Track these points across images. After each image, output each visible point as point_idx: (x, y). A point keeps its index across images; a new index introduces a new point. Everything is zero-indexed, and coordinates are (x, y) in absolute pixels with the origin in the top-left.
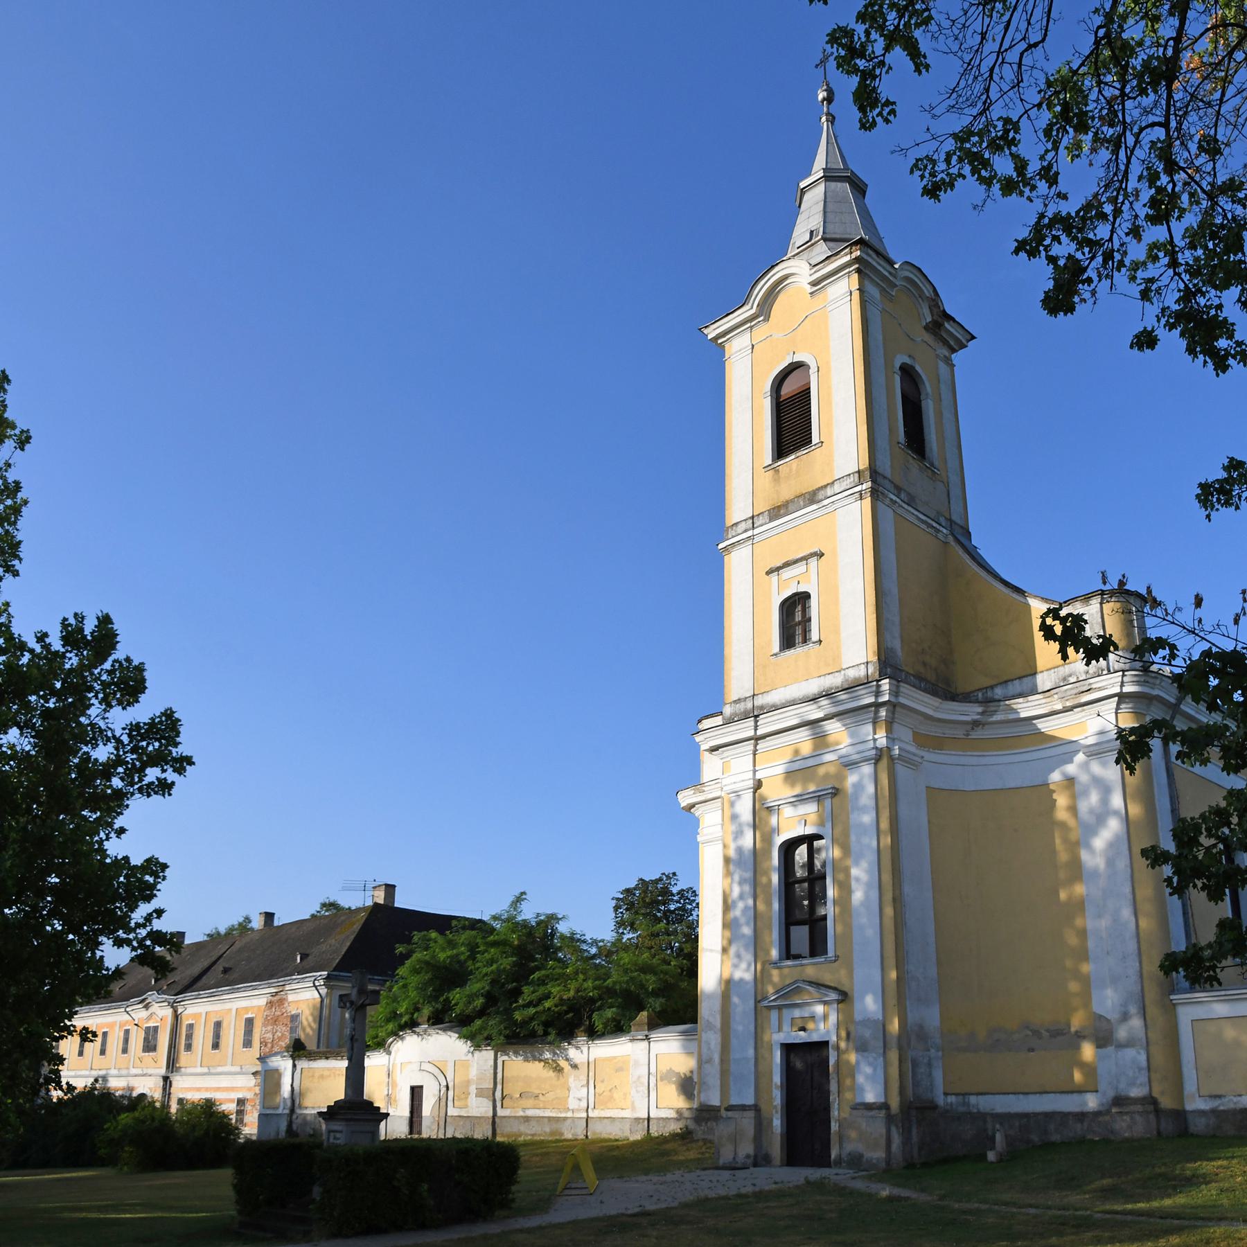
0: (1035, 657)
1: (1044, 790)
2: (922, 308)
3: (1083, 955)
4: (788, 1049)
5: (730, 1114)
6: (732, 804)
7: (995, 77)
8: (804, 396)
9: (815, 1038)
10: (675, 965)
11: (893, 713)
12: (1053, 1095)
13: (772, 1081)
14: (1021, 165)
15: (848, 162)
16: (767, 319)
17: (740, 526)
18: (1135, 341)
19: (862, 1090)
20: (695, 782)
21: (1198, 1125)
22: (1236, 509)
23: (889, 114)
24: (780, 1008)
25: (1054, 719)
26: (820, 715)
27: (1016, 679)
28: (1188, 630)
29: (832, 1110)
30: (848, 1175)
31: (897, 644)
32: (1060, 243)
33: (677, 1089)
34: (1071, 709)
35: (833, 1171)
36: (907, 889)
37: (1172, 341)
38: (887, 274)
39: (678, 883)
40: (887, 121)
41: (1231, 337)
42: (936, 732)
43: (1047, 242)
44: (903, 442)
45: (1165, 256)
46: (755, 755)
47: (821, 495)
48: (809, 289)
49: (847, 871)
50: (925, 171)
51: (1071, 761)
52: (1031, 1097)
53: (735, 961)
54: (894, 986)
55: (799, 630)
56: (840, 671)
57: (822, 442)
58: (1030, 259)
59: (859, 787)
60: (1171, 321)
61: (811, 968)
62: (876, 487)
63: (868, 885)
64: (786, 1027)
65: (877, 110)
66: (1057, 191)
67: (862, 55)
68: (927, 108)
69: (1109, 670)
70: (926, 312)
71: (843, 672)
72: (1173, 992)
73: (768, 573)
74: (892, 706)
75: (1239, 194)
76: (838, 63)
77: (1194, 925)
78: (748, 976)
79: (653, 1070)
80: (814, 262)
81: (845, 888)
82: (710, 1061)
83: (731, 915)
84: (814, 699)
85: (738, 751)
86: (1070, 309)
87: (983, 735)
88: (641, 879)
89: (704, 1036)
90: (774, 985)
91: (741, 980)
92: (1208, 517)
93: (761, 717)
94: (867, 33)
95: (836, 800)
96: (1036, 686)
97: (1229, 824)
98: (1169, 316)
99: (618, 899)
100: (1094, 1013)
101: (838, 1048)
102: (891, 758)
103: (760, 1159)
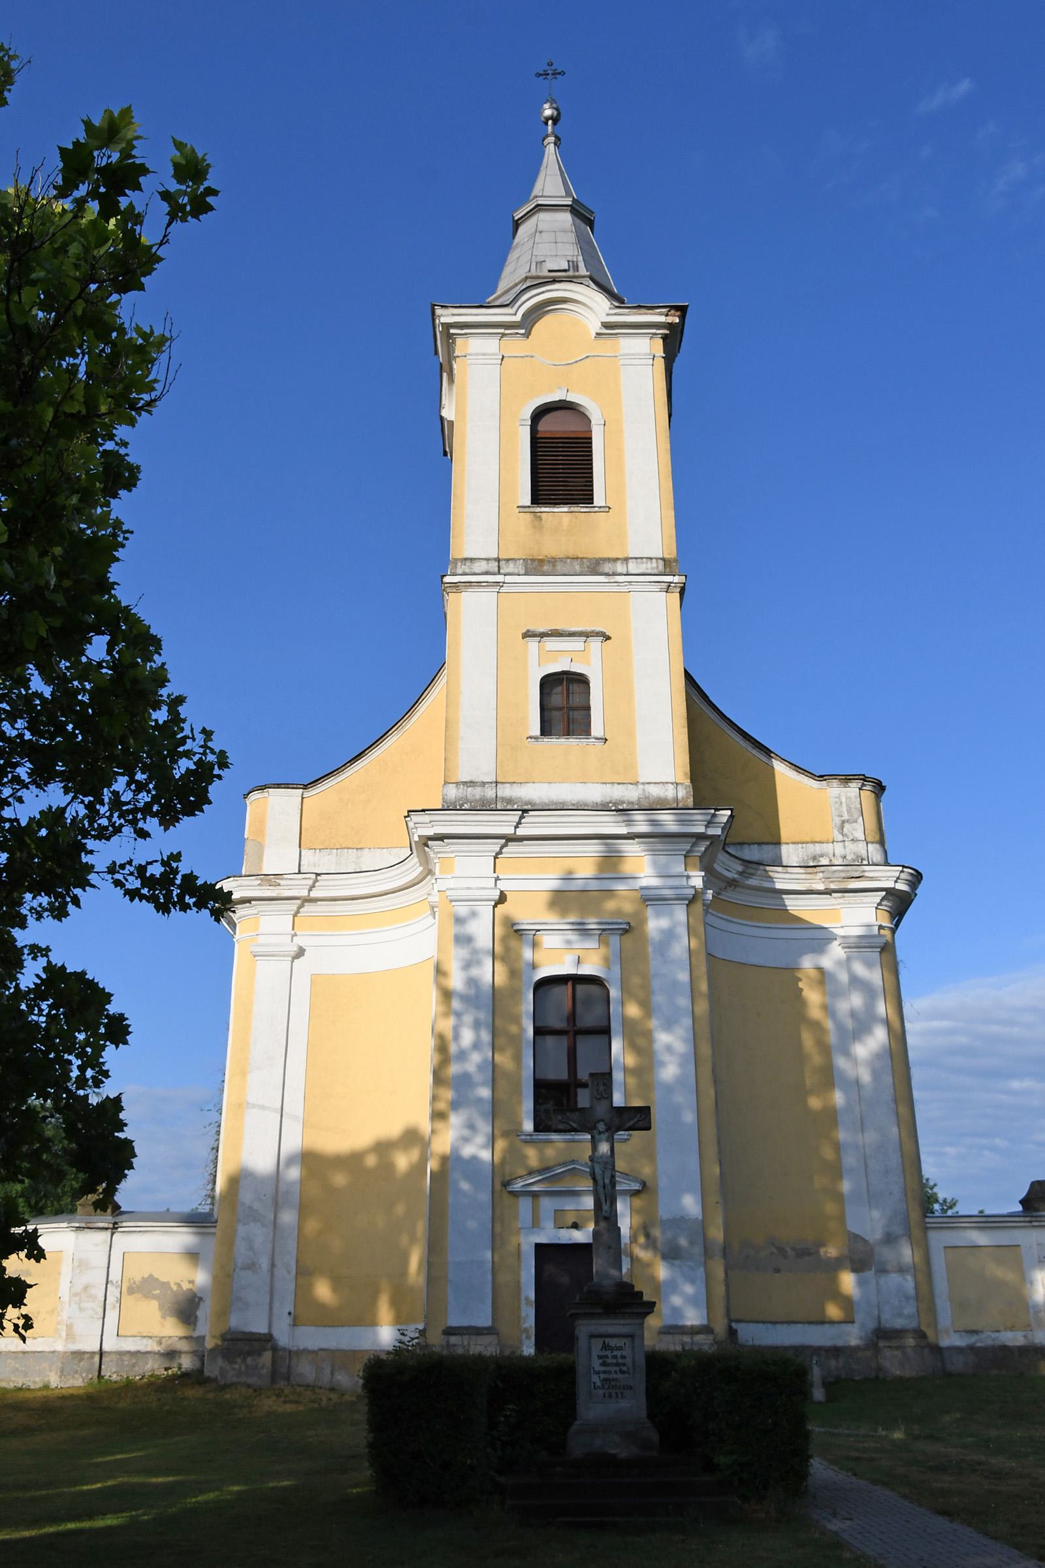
1: (791, 973)
4: (541, 1250)
16: (527, 335)
25: (804, 899)
27: (754, 844)
49: (648, 1035)
52: (778, 1326)
53: (466, 1132)
59: (669, 935)
73: (528, 635)
79: (115, 1275)
91: (474, 1159)
93: (531, 813)
100: (849, 1231)
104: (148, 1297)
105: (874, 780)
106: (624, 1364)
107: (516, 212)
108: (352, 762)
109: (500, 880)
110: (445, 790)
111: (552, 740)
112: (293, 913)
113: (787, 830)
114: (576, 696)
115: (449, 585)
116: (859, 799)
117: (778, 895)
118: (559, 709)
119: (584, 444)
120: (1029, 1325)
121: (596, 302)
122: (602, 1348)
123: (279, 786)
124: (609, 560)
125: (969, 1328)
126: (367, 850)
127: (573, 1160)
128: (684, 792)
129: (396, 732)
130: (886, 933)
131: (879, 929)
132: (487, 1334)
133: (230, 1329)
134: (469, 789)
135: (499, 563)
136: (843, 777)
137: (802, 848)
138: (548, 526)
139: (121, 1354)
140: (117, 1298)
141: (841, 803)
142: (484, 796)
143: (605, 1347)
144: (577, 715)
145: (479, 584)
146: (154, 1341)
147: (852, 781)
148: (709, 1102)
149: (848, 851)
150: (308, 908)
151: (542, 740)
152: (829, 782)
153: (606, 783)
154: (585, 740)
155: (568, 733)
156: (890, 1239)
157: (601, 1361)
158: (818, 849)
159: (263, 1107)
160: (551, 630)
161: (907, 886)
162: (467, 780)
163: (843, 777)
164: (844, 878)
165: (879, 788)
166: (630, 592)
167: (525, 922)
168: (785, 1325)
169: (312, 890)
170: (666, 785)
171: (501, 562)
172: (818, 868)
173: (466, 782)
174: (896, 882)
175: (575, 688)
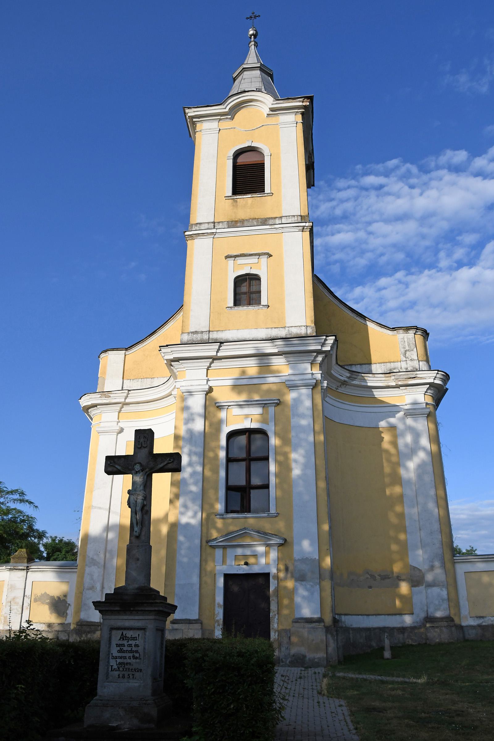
0: (370, 355)
3: (404, 529)
4: (228, 577)
5: (176, 626)
9: (256, 569)
12: (383, 616)
16: (232, 118)
17: (203, 225)
19: (299, 607)
24: (224, 547)
25: (385, 391)
27: (358, 364)
29: (271, 623)
49: (286, 455)
53: (182, 510)
59: (297, 401)
63: (305, 466)
64: (228, 562)
73: (227, 257)
79: (28, 593)
91: (188, 525)
93: (225, 344)
101: (277, 577)
104: (44, 604)
105: (422, 329)
106: (137, 652)
107: (233, 74)
108: (150, 336)
109: (210, 381)
110: (182, 337)
111: (240, 308)
112: (118, 411)
113: (374, 357)
114: (254, 287)
115: (188, 236)
116: (414, 339)
118: (245, 293)
119: (260, 167)
121: (267, 99)
122: (121, 638)
123: (113, 350)
124: (272, 218)
125: (478, 615)
126: (156, 378)
127: (245, 528)
128: (311, 330)
129: (172, 320)
130: (431, 408)
131: (426, 405)
133: (80, 620)
134: (195, 335)
135: (214, 224)
136: (405, 328)
137: (384, 365)
138: (240, 205)
140: (29, 604)
141: (405, 341)
142: (202, 338)
143: (123, 637)
144: (254, 296)
145: (203, 234)
146: (46, 625)
147: (410, 330)
149: (408, 365)
150: (126, 408)
151: (234, 308)
152: (398, 331)
153: (268, 328)
154: (257, 307)
155: (249, 304)
157: (118, 648)
159: (100, 508)
160: (240, 254)
161: (441, 382)
162: (194, 331)
163: (405, 328)
164: (406, 378)
165: (425, 334)
166: (283, 233)
167: (222, 401)
168: (375, 616)
169: (126, 399)
170: (301, 327)
171: (215, 224)
172: (391, 374)
173: (193, 332)
174: (434, 379)
175: (254, 282)
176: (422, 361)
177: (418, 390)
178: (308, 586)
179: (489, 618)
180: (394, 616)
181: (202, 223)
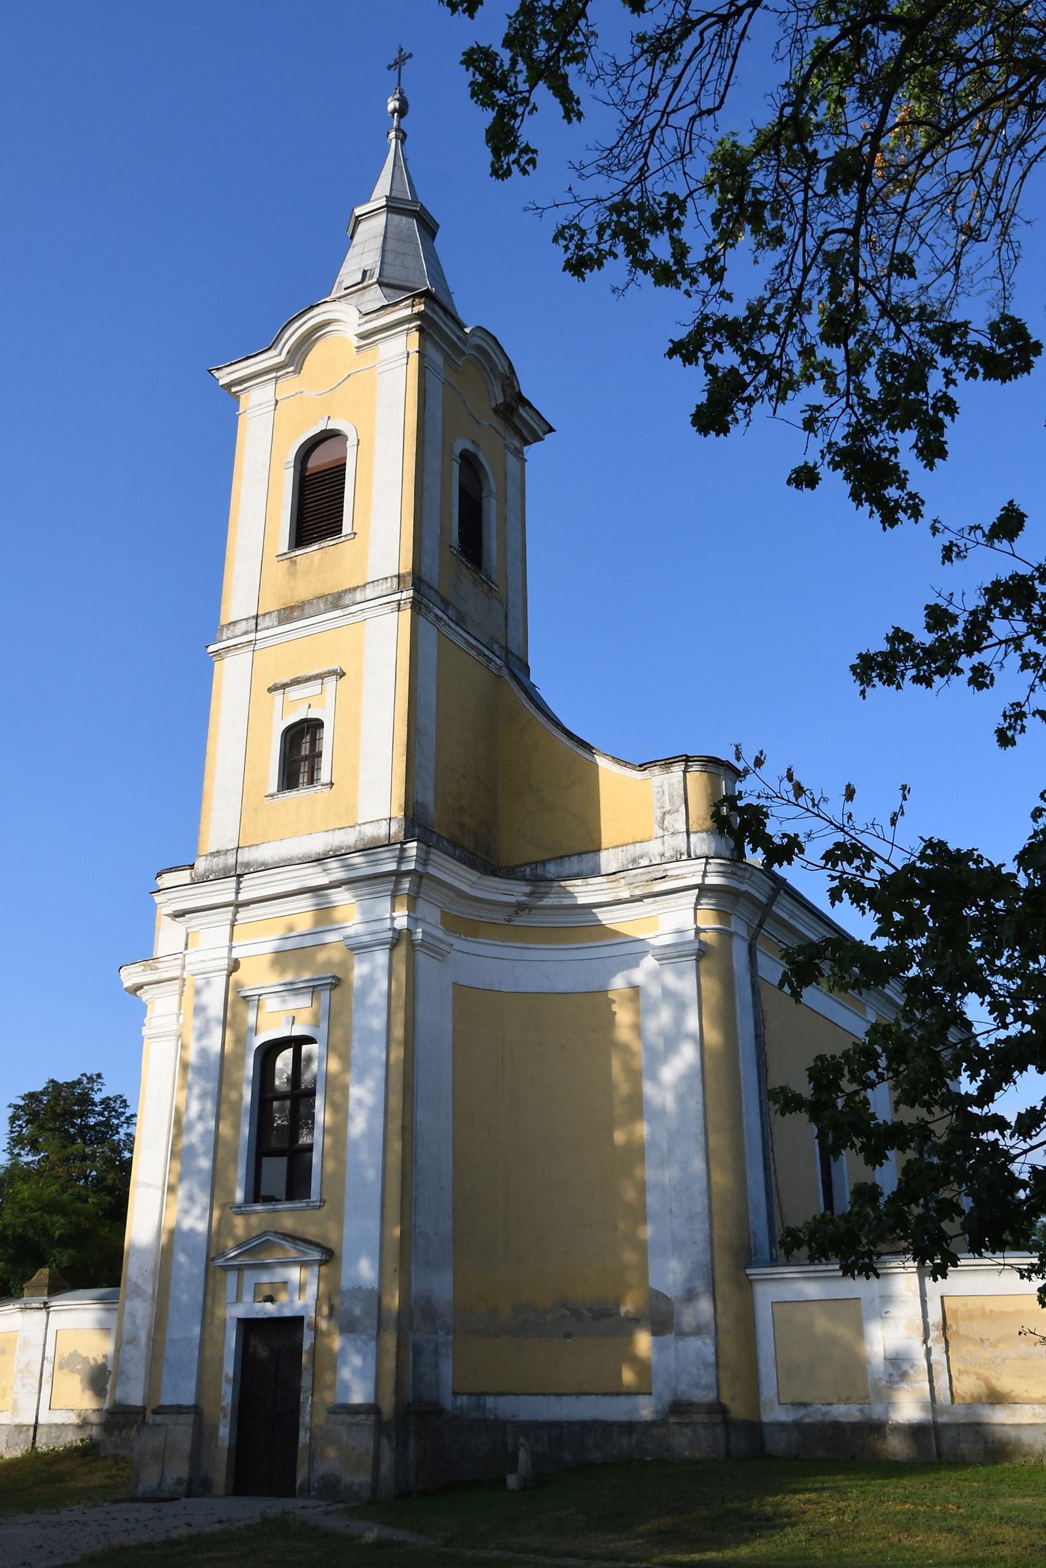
2: (493, 386)
4: (248, 1326)
5: (159, 1419)
6: (198, 992)
7: (656, 141)
8: (337, 473)
9: (287, 1313)
10: (93, 1203)
11: (419, 886)
12: (593, 1397)
13: (222, 1373)
14: (680, 250)
15: (418, 194)
16: (298, 370)
18: (793, 476)
20: (147, 957)
21: (777, 1443)
22: (897, 689)
23: (528, 162)
24: (240, 1269)
25: (618, 910)
26: (324, 881)
27: (574, 855)
28: (836, 826)
29: (301, 1414)
30: (319, 1509)
31: (429, 798)
32: (721, 352)
33: (81, 1382)
34: (641, 899)
35: (299, 1502)
36: (421, 1115)
37: (834, 483)
38: (455, 338)
39: (103, 1088)
40: (524, 172)
41: (902, 486)
42: (470, 914)
43: (708, 348)
44: (457, 547)
45: (822, 378)
46: (233, 926)
47: (347, 599)
48: (356, 342)
49: (345, 1090)
50: (571, 241)
51: (637, 965)
52: (565, 1399)
53: (186, 1204)
54: (397, 1244)
55: (304, 767)
56: (354, 826)
57: (355, 534)
58: (685, 366)
59: (369, 980)
60: (837, 459)
61: (288, 1217)
62: (419, 597)
63: (372, 1110)
64: (248, 1297)
65: (513, 157)
66: (721, 289)
67: (502, 86)
68: (577, 166)
69: (689, 855)
70: (498, 391)
71: (358, 828)
72: (750, 1265)
73: (270, 690)
74: (418, 876)
75: (928, 325)
76: (473, 91)
77: (776, 1185)
78: (202, 1227)
79: (49, 1353)
80: (365, 310)
81: (340, 1109)
82: (133, 1341)
83: (185, 1141)
84: (319, 860)
85: (212, 919)
86: (723, 429)
87: (529, 922)
88: (53, 1081)
89: (129, 1305)
90: (235, 1238)
91: (192, 1231)
92: (863, 692)
94: (514, 62)
95: (335, 993)
96: (599, 866)
97: (876, 1067)
98: (835, 454)
99: (17, 1107)
101: (315, 1328)
102: (412, 944)
103: (197, 1486)
113: (607, 836)
117: (588, 910)
120: (867, 1397)
125: (798, 1400)
132: (187, 1413)
139: (50, 1426)
148: (395, 1159)
149: (666, 845)
156: (690, 1296)
158: (638, 849)
168: (574, 1397)
176: (697, 832)
177: (680, 901)
178: (360, 1343)
179: (818, 1406)
180: (615, 1398)
181: (237, 621)
